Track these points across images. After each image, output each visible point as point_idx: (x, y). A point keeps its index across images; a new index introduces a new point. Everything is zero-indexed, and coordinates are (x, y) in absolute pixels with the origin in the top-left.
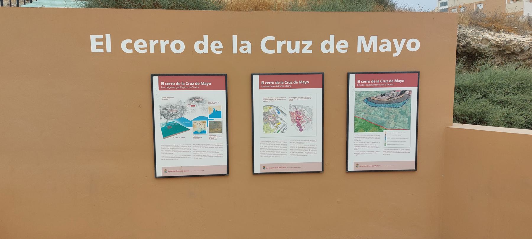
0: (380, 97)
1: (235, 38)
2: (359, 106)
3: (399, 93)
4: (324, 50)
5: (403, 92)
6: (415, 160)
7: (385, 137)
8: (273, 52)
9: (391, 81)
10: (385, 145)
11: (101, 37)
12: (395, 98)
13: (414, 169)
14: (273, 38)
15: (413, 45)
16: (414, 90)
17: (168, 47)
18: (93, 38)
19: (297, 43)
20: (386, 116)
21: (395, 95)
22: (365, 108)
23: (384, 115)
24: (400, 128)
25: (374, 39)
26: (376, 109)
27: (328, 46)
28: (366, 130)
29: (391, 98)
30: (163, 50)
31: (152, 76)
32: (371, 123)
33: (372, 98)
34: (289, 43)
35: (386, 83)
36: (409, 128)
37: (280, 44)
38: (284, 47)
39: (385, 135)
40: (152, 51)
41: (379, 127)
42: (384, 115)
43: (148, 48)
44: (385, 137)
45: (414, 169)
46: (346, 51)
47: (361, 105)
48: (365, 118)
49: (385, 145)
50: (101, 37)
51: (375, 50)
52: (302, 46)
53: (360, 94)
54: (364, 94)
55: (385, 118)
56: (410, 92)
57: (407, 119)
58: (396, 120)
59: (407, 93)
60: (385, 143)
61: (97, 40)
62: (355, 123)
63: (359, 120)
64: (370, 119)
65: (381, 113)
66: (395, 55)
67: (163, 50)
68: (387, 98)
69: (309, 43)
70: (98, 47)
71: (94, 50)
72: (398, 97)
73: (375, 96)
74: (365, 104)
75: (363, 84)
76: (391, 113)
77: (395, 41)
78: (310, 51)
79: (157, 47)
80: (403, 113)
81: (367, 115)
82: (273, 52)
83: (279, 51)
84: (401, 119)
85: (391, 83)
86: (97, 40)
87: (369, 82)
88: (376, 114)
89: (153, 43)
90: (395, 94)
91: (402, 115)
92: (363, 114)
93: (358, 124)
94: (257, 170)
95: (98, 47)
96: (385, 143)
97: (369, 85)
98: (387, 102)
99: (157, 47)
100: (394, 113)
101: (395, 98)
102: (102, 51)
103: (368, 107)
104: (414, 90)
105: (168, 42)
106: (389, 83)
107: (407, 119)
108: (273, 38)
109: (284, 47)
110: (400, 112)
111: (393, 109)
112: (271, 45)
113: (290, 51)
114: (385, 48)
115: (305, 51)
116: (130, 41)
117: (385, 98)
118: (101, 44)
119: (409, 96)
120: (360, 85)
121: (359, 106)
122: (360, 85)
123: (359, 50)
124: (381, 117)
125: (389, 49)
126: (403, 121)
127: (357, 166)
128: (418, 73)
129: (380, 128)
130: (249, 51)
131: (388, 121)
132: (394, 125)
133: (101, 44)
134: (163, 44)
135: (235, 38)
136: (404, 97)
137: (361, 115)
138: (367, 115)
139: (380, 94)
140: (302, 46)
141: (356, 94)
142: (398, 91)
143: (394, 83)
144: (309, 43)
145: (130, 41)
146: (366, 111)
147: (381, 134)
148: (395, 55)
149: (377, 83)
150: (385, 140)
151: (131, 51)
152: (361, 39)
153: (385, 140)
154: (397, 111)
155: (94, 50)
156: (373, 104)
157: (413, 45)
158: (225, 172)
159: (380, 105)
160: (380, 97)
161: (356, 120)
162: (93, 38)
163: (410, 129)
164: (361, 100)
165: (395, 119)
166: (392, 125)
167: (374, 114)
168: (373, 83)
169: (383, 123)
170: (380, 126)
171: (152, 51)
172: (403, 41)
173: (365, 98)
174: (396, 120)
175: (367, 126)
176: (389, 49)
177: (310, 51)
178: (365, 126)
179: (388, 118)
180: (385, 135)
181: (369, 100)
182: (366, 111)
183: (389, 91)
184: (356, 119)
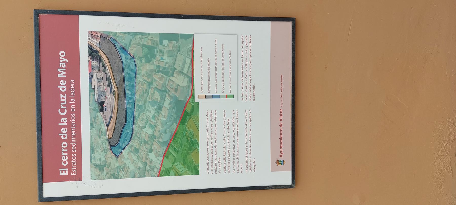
0: (108, 113)
1: (59, 124)
2: (132, 168)
3: (95, 63)
4: (65, 90)
5: (93, 54)
6: (268, 23)
7: (212, 97)
8: (66, 110)
9: (62, 86)
10: (231, 96)
11: (61, 172)
12: (110, 75)
13: (290, 24)
14: (59, 110)
15: (62, 54)
16: (87, 24)
17: (64, 149)
18: (61, 174)
19: (61, 100)
20: (157, 96)
21: (101, 75)
22: (136, 151)
23: (154, 102)
24: (189, 61)
25: (59, 70)
26: (139, 123)
27: (64, 136)
28: (193, 144)
29: (109, 85)
30: (66, 150)
31: (42, 199)
32: (174, 135)
33: (109, 134)
34: (61, 104)
35: (68, 99)
36: (190, 37)
37: (62, 107)
38: (63, 106)
39: (207, 97)
40: (67, 154)
41: (186, 113)
42: (154, 102)
43: (66, 156)
44: (212, 97)
45: (290, 24)
46: (66, 129)
47: (128, 163)
48: (162, 150)
49: (231, 96)
50: (61, 172)
51: (65, 69)
52: (63, 98)
53: (100, 169)
54: (100, 155)
55: (163, 98)
56: (92, 35)
57: (165, 42)
58: (168, 72)
59: (95, 43)
60: (227, 97)
61: (62, 173)
62: (177, 173)
63: (168, 164)
64: (166, 137)
65: (151, 111)
66: (67, 61)
67: (66, 150)
68: (109, 96)
69: (61, 95)
70: (65, 172)
71: (67, 174)
72: (107, 66)
73: (104, 128)
74: (125, 152)
75: (70, 160)
76: (150, 84)
77: (60, 61)
78: (65, 95)
79: (65, 152)
80: (150, 53)
81: (155, 146)
82: (66, 110)
83: (65, 107)
84: (167, 59)
85: (68, 85)
86: (62, 173)
87: (64, 145)
88: (152, 122)
89: (63, 154)
90: (99, 75)
91: (154, 56)
92: (152, 156)
93: (179, 166)
94: (285, 178)
95: (65, 172)
96: (227, 97)
97: (74, 143)
98: (121, 93)
99: (65, 152)
100: (149, 76)
101: (110, 75)
102: (67, 172)
103: (135, 143)
104: (87, 24)
105: (62, 148)
106: (68, 92)
107: (165, 42)
108: (59, 110)
109: (63, 106)
110: (148, 61)
111: (139, 79)
112: (63, 111)
113: (65, 103)
114: (65, 120)
115: (65, 97)
116: (63, 162)
117: (110, 101)
118: (64, 172)
119: (104, 37)
120: (74, 169)
121: (132, 168)
122: (74, 169)
123: (65, 76)
124: (160, 108)
125: (64, 64)
126: (172, 54)
127: (280, 163)
128: (37, 13)
129: (188, 110)
130: (66, 119)
131: (172, 92)
132: (181, 77)
133: (64, 172)
134: (63, 150)
135: (59, 124)
136: (107, 50)
137: (155, 159)
138: (155, 146)
139: (100, 115)
140: (63, 98)
141: (98, 177)
142: (91, 68)
143: (67, 79)
144: (61, 95)
145: (63, 162)
146: (143, 149)
147: (205, 107)
148: (67, 61)
149: (69, 123)
150: (218, 97)
151: (67, 162)
152: (59, 76)
153: (218, 97)
154: (145, 68)
155: (67, 174)
156: (126, 131)
157: (62, 54)
158: (289, 25)
159: (129, 112)
160: (108, 113)
161: (167, 173)
162: (61, 174)
163: (191, 36)
164: (115, 163)
165: (167, 73)
166: (181, 81)
167: (154, 127)
168: (69, 133)
169: (176, 103)
170: (184, 111)
171: (67, 154)
172: (60, 58)
173: (110, 153)
174: (168, 72)
175: (185, 143)
176: (64, 64)
177: (65, 95)
178: (183, 148)
179: (163, 91)
180: (207, 97)
181: (117, 141)
182: (143, 149)
183: (92, 90)
184: (164, 172)
